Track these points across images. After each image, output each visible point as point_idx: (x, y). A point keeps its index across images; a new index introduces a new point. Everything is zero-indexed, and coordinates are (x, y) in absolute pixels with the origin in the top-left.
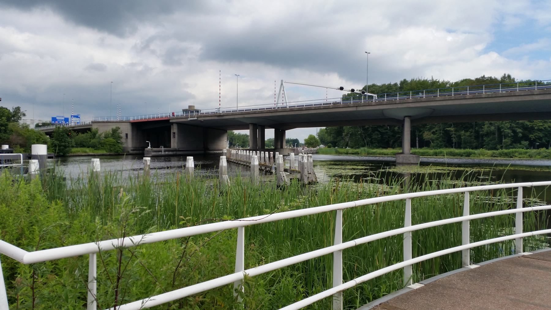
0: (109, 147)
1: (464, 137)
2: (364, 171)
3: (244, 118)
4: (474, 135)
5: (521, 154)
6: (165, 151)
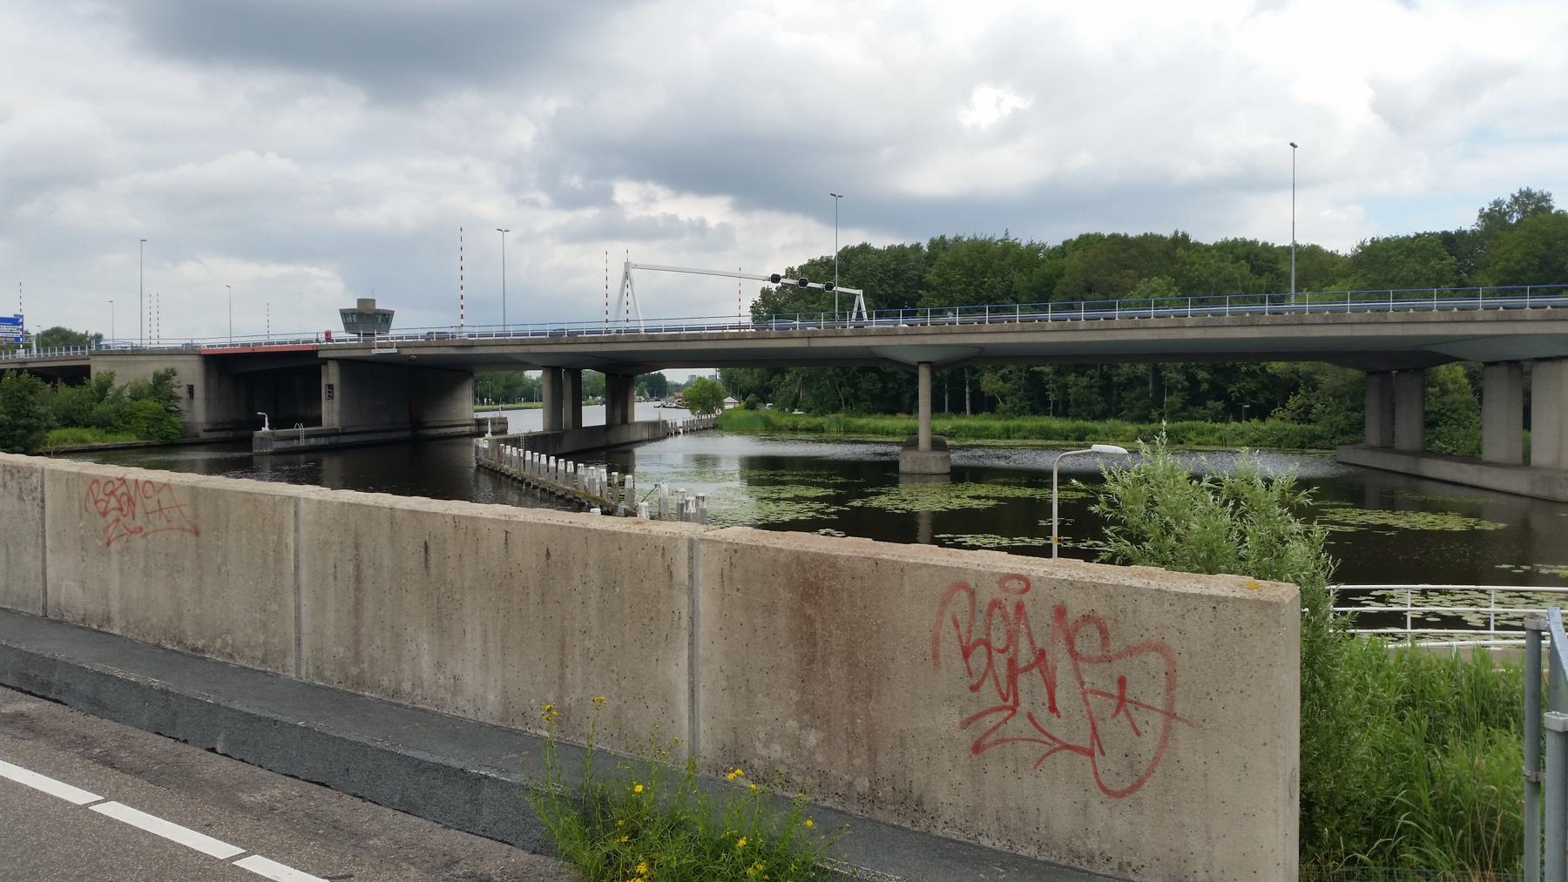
0: (145, 425)
1: (1074, 389)
2: (816, 506)
4: (1098, 384)
5: (1201, 433)
6: (308, 436)
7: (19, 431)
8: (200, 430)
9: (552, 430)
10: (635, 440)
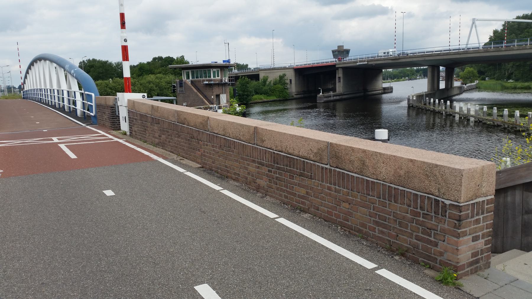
3: (425, 60)
6: (334, 96)
7: (245, 96)
8: (294, 94)
9: (431, 91)
10: (454, 94)
